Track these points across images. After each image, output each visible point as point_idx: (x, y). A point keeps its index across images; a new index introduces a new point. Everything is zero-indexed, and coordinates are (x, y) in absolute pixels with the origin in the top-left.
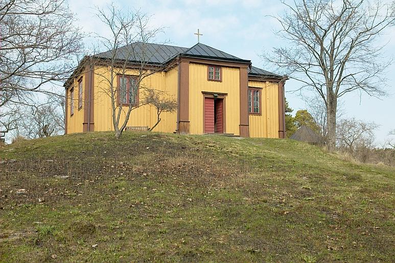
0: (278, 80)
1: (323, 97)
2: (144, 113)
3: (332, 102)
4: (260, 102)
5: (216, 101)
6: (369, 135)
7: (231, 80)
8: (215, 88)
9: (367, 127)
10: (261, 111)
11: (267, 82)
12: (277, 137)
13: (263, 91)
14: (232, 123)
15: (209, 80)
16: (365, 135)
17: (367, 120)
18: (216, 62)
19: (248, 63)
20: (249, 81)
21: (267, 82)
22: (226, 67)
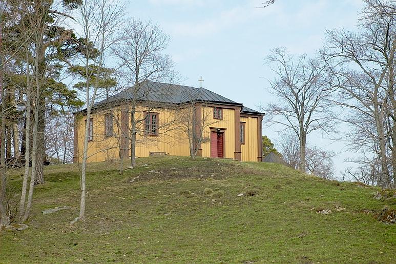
0: (258, 116)
1: (298, 135)
2: (31, 153)
3: (303, 137)
4: (244, 133)
5: (219, 134)
6: (328, 163)
7: (229, 115)
8: (219, 125)
9: (327, 155)
10: (244, 142)
11: (250, 118)
12: (257, 161)
13: (246, 125)
14: (229, 152)
15: (215, 119)
16: (325, 162)
17: (327, 150)
18: (220, 105)
19: (240, 105)
20: (241, 117)
21: (250, 118)
22: (226, 108)
